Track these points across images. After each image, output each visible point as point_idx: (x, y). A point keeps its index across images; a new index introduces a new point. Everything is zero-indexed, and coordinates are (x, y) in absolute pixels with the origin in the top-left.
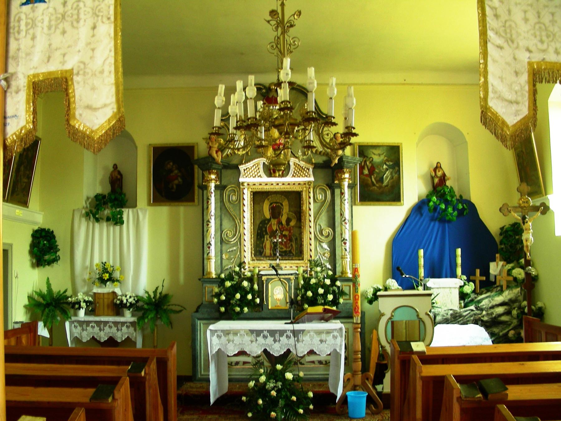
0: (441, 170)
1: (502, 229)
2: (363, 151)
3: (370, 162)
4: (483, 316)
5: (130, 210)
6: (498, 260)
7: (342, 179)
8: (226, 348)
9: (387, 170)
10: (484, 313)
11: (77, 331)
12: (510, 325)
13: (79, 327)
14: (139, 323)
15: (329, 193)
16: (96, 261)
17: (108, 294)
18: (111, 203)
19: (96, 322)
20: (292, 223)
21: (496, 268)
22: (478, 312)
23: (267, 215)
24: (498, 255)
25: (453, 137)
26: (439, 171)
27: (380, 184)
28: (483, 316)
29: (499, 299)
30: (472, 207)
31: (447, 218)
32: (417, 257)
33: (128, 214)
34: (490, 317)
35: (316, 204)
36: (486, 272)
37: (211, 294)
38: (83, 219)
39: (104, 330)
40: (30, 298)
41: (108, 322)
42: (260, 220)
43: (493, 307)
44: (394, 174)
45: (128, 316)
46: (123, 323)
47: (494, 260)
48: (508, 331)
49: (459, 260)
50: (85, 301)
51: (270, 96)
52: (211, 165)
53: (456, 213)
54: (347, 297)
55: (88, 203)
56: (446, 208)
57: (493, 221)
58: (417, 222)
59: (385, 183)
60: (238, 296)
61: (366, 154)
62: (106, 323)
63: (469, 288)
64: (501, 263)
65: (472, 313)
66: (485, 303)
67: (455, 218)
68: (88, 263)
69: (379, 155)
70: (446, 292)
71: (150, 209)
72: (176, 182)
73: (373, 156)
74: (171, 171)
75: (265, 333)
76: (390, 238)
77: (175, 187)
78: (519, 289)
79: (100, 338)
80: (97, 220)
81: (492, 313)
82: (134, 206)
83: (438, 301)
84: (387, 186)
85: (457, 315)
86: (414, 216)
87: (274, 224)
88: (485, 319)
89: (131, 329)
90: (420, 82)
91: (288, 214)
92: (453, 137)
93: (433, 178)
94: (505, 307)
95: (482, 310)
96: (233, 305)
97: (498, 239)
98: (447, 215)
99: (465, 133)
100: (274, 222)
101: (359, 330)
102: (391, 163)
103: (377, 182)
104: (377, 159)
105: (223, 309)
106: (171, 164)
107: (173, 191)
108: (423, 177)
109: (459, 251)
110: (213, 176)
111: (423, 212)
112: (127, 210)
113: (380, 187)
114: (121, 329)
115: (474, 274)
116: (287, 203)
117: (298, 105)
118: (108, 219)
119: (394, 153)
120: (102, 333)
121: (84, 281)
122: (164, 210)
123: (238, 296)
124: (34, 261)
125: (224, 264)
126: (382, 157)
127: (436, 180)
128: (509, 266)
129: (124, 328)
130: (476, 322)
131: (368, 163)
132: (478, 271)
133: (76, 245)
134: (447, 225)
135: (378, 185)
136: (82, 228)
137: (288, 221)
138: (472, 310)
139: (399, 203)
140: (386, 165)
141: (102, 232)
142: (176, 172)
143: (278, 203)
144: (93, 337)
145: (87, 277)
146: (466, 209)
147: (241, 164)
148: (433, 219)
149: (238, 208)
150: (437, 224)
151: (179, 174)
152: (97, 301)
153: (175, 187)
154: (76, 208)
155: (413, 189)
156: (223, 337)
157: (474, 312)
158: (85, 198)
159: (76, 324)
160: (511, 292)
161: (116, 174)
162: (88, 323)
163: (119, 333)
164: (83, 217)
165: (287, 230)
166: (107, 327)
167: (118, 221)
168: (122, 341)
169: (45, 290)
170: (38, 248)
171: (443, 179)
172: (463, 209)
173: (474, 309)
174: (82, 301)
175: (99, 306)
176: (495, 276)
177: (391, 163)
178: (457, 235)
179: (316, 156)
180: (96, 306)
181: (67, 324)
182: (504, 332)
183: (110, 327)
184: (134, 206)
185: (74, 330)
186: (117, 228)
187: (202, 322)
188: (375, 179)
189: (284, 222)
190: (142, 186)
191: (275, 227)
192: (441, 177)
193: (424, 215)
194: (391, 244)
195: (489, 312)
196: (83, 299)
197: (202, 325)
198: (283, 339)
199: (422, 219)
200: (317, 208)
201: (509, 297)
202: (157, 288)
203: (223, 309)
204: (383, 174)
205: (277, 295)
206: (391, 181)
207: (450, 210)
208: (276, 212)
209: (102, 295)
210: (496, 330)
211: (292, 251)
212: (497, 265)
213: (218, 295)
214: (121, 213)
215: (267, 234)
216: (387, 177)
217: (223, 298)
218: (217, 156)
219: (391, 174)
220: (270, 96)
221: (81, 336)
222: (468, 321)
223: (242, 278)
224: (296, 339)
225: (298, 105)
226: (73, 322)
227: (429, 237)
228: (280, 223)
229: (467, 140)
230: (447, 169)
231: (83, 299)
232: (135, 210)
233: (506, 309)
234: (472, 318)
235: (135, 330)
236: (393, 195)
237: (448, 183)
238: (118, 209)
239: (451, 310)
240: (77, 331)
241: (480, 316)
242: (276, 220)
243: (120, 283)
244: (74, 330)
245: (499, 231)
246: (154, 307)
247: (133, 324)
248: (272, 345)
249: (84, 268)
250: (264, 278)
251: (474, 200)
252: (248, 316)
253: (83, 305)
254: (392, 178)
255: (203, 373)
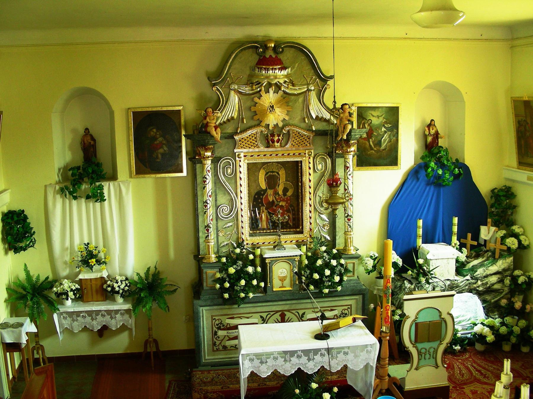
0: (434, 128)
1: (493, 191)
2: (361, 113)
3: (369, 125)
4: (478, 287)
5: (112, 184)
6: (489, 225)
7: (347, 152)
8: (259, 371)
9: (385, 132)
10: (479, 283)
11: (67, 323)
12: (502, 293)
13: (68, 318)
14: (134, 310)
15: (329, 161)
16: (77, 241)
17: (96, 279)
18: (87, 174)
19: (86, 312)
20: (289, 193)
21: (486, 232)
22: (473, 281)
23: (263, 186)
24: (489, 220)
25: (448, 95)
26: (433, 129)
27: (378, 147)
28: (478, 287)
29: (494, 268)
30: (466, 169)
31: (444, 184)
32: (416, 227)
33: (109, 188)
34: (485, 287)
35: (316, 174)
36: (476, 236)
37: (213, 279)
38: (58, 197)
39: (96, 318)
40: (8, 289)
41: (100, 311)
42: (256, 192)
43: (487, 276)
44: (392, 137)
45: (121, 304)
46: (117, 312)
47: (486, 225)
48: (499, 300)
49: (455, 229)
50: (72, 290)
51: (267, 56)
52: (208, 142)
53: (452, 178)
54: (351, 274)
55: (60, 175)
56: (444, 173)
57: (485, 181)
58: (415, 185)
59: (383, 147)
60: (243, 282)
61: (365, 117)
62: (98, 312)
63: (463, 257)
64: (493, 229)
65: (468, 282)
66: (480, 272)
67: (451, 183)
68: (67, 244)
69: (378, 117)
70: (442, 258)
71: (134, 182)
72: (161, 151)
73: (372, 118)
74: (155, 138)
75: (299, 353)
76: (386, 203)
77: (160, 156)
78: (512, 258)
79: (93, 326)
80: (75, 198)
81: (487, 283)
82: (113, 177)
83: (437, 273)
84: (383, 150)
85: (455, 285)
86: (411, 181)
87: (270, 195)
88: (481, 289)
89: (126, 317)
90: (422, 37)
91: (284, 184)
92: (448, 95)
93: (425, 136)
94: (498, 276)
95: (477, 279)
96: (237, 291)
97: (487, 199)
98: (444, 181)
99: (463, 93)
100: (270, 192)
101: (388, 337)
102: (390, 126)
103: (375, 145)
104: (375, 121)
105: (226, 296)
106: (155, 130)
107: (158, 160)
108: (416, 132)
109: (455, 220)
110: (209, 154)
111: (419, 176)
112: (107, 183)
113: (378, 151)
114: (115, 317)
115: (466, 238)
116: (284, 172)
117: (297, 64)
118: (88, 197)
119: (393, 112)
120: (94, 322)
121: (66, 263)
122: (149, 181)
123: (243, 282)
124: (7, 246)
125: (220, 242)
126: (381, 119)
127: (430, 139)
128: (502, 233)
129: (118, 316)
130: (470, 291)
131: (366, 126)
132: (469, 235)
133: (52, 225)
134: (442, 189)
135: (375, 149)
136: (58, 206)
137: (285, 190)
138: (468, 280)
139: (395, 167)
140: (385, 127)
141: (81, 209)
142: (160, 139)
143: (273, 172)
144: (85, 326)
145: (67, 258)
146: (462, 174)
147: (236, 133)
148: (428, 184)
149: (233, 181)
150: (432, 188)
151: (164, 142)
152: (84, 287)
153: (160, 156)
154: (48, 183)
155: (409, 152)
156: (256, 360)
157: (469, 282)
158: (57, 171)
159: (65, 315)
160: (504, 261)
161: (89, 138)
162: (78, 314)
163: (113, 321)
164: (57, 194)
165: (283, 200)
166: (100, 316)
167: (97, 196)
168: (117, 329)
169: (23, 276)
170: (12, 235)
171: (437, 136)
172: (460, 174)
173: (470, 279)
174: (69, 290)
175: (87, 292)
176: (485, 241)
177: (390, 126)
178: (448, 197)
179: (316, 122)
180: (83, 292)
181: (55, 316)
182: (496, 299)
183: (103, 316)
184: (113, 177)
185: (64, 322)
186: (98, 204)
187: (204, 308)
188: (373, 143)
189: (281, 192)
190: (124, 157)
191: (271, 197)
192: (434, 135)
193: (420, 179)
194: (386, 209)
195: (484, 282)
196: (70, 287)
197: (204, 311)
198: (318, 358)
199: (418, 183)
200: (317, 178)
201: (503, 267)
202: (149, 269)
203: (226, 296)
204: (381, 137)
205: (281, 275)
206: (389, 144)
207: (447, 176)
208: (272, 181)
209: (89, 282)
210: (488, 297)
211: (289, 222)
212: (489, 230)
213: (221, 281)
214: (101, 188)
215: (263, 205)
216: (385, 140)
217: (227, 285)
218: (217, 133)
219: (389, 137)
220: (267, 56)
221: (72, 328)
222: (463, 290)
223: (247, 262)
224: (330, 356)
225: (297, 64)
226: (61, 314)
227: (423, 202)
228: (276, 193)
229: (465, 100)
230: (439, 126)
231: (70, 287)
232: (116, 183)
233: (499, 278)
234: (467, 287)
235: (130, 317)
236: (391, 159)
237: (441, 142)
238: (98, 184)
239: (448, 280)
240: (67, 323)
241: (475, 286)
242: (272, 191)
243: (106, 264)
244: (64, 322)
245: (491, 194)
246: (148, 289)
247: (128, 311)
248: (306, 364)
249: (64, 249)
250: (267, 261)
251: (468, 162)
252: (252, 301)
253: (71, 294)
254: (390, 141)
255: (207, 357)
